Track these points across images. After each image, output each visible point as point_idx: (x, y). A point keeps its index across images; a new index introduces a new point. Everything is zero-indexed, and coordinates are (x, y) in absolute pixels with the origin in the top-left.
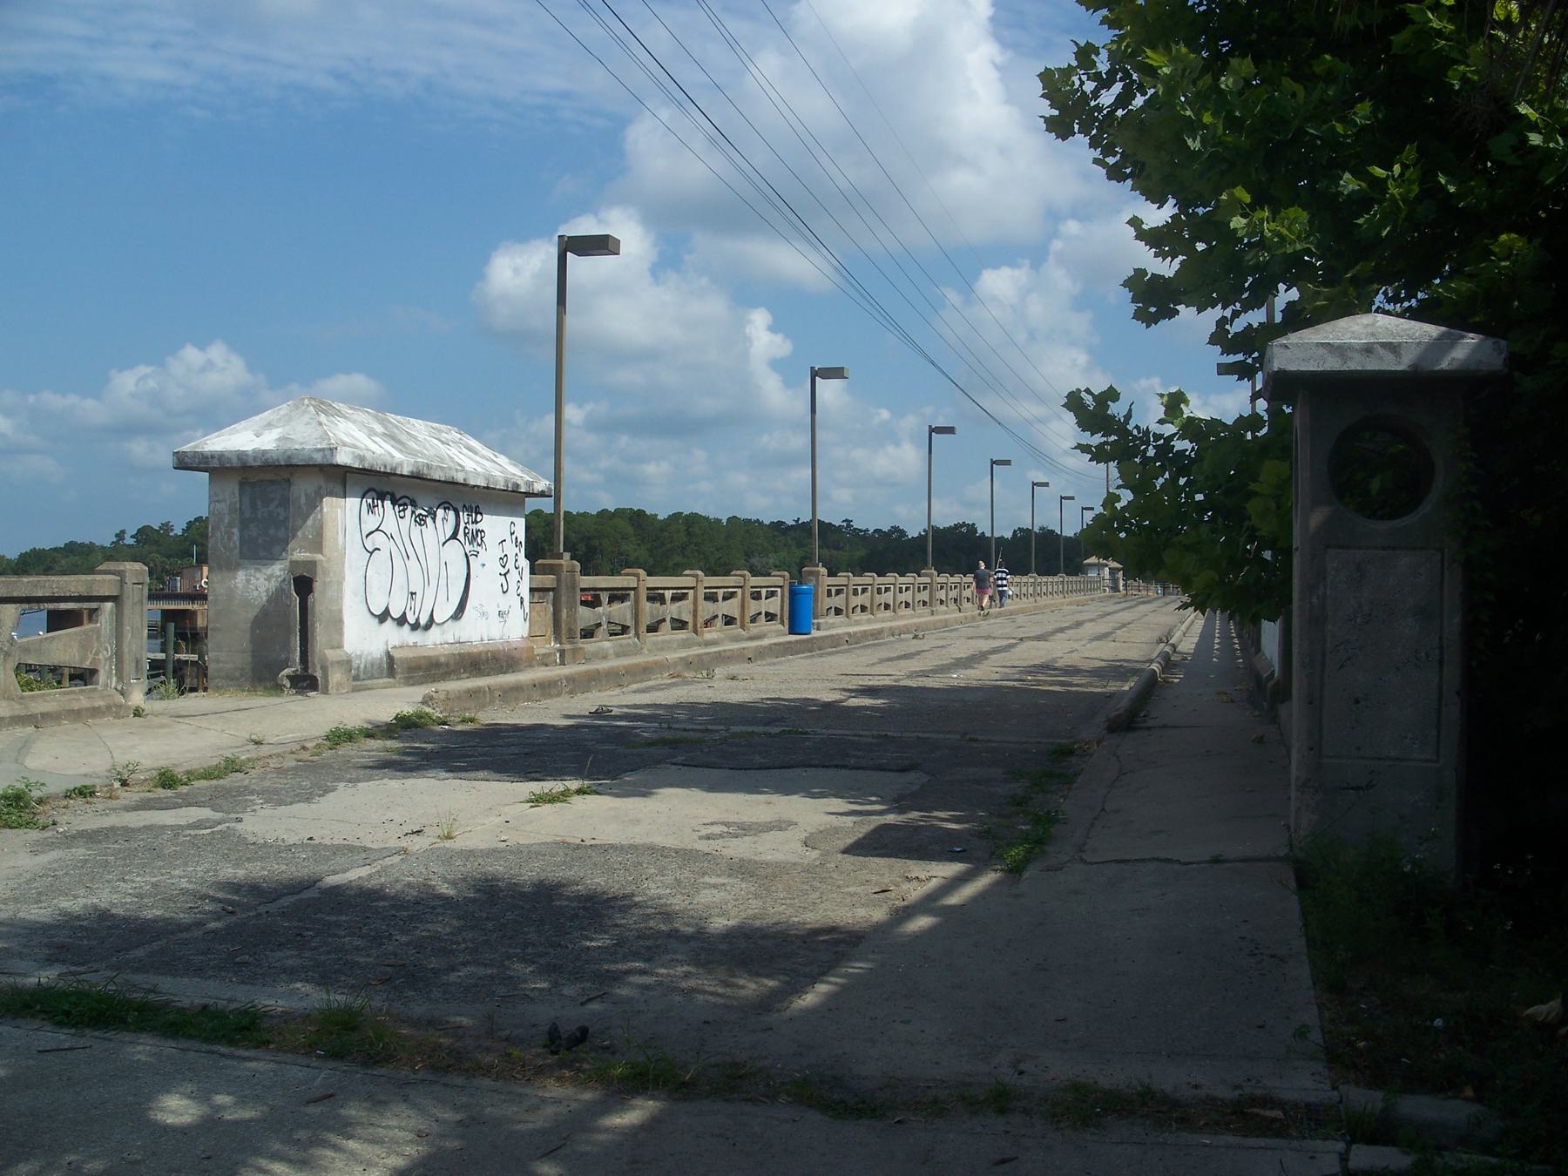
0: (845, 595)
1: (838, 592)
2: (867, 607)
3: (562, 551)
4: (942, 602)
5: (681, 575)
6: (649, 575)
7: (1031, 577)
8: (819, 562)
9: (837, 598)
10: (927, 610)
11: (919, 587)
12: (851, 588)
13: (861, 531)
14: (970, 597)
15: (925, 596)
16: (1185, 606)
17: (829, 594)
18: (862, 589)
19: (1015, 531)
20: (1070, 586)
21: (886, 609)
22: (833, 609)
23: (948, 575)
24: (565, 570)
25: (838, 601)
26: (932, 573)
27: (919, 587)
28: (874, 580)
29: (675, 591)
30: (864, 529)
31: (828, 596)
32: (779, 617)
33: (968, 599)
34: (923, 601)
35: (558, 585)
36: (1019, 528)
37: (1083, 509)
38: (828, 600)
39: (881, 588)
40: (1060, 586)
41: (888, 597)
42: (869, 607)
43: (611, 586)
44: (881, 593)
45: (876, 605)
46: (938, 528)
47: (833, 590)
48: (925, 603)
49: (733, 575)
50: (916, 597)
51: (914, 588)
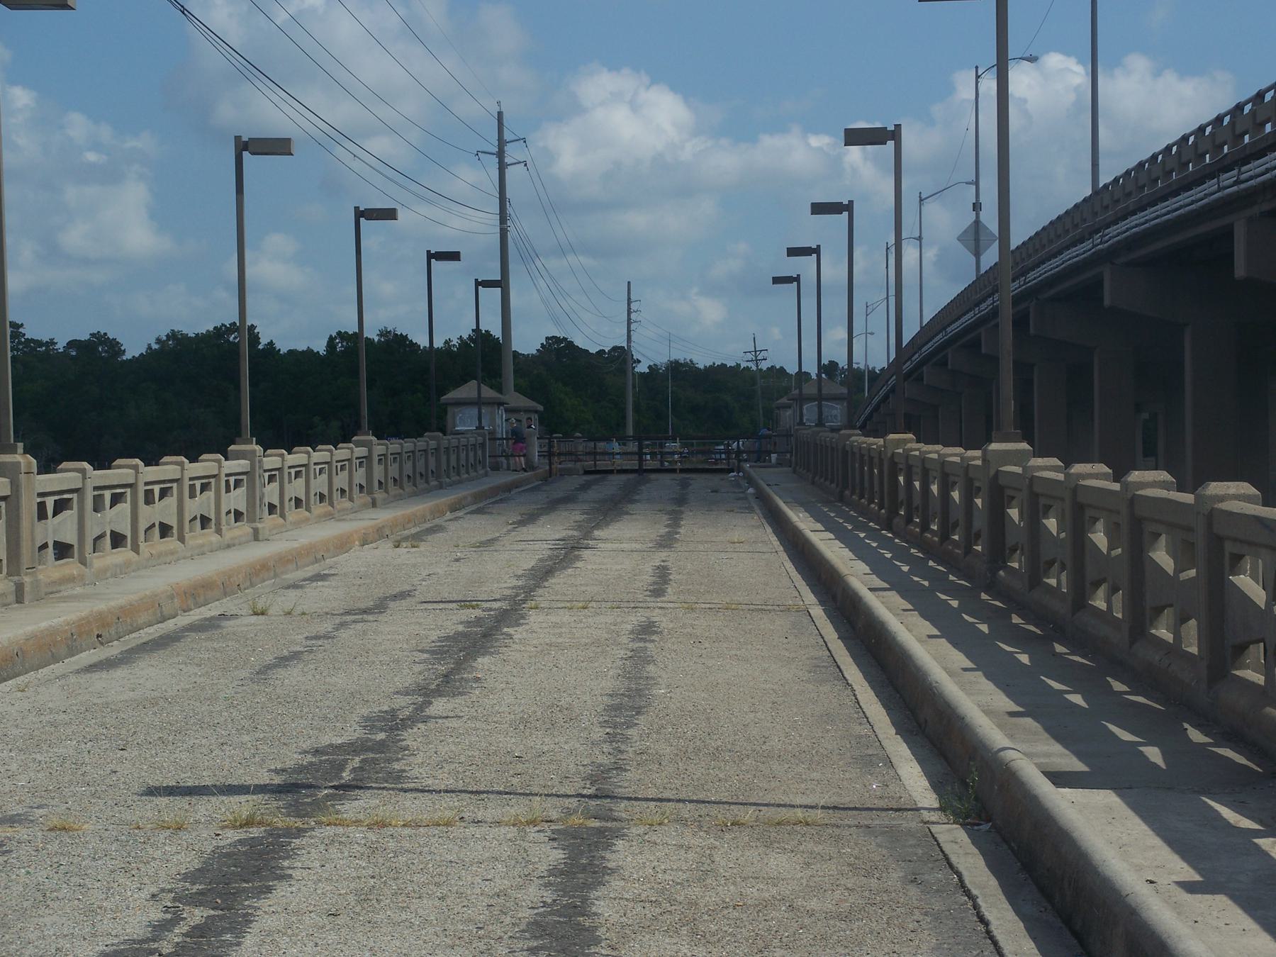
0: (278, 483)
1: (60, 506)
2: (124, 537)
3: (12, 441)
4: (272, 508)
5: (55, 472)
6: (356, 447)
7: (358, 444)
8: (252, 435)
9: (60, 517)
10: (244, 529)
11: (227, 482)
12: (142, 489)
13: (39, 343)
14: (326, 493)
15: (237, 499)
16: (714, 364)
17: (42, 514)
18: (162, 490)
19: (331, 339)
20: (453, 457)
21: (163, 535)
22: (199, 520)
23: (140, 463)
24: (23, 471)
25: (64, 527)
26: (254, 452)
27: (227, 482)
28: (84, 478)
29: (57, 498)
30: (45, 339)
31: (96, 510)
32: (213, 521)
33: (343, 491)
34: (236, 511)
35: (219, 472)
36: (339, 333)
37: (430, 256)
38: (40, 526)
39: (152, 491)
40: (480, 453)
41: (117, 519)
42: (175, 525)
43: (59, 489)
44: (46, 518)
45: (143, 526)
46: (185, 337)
47: (50, 502)
48: (238, 515)
49: (202, 461)
50: (88, 523)
51: (134, 495)
